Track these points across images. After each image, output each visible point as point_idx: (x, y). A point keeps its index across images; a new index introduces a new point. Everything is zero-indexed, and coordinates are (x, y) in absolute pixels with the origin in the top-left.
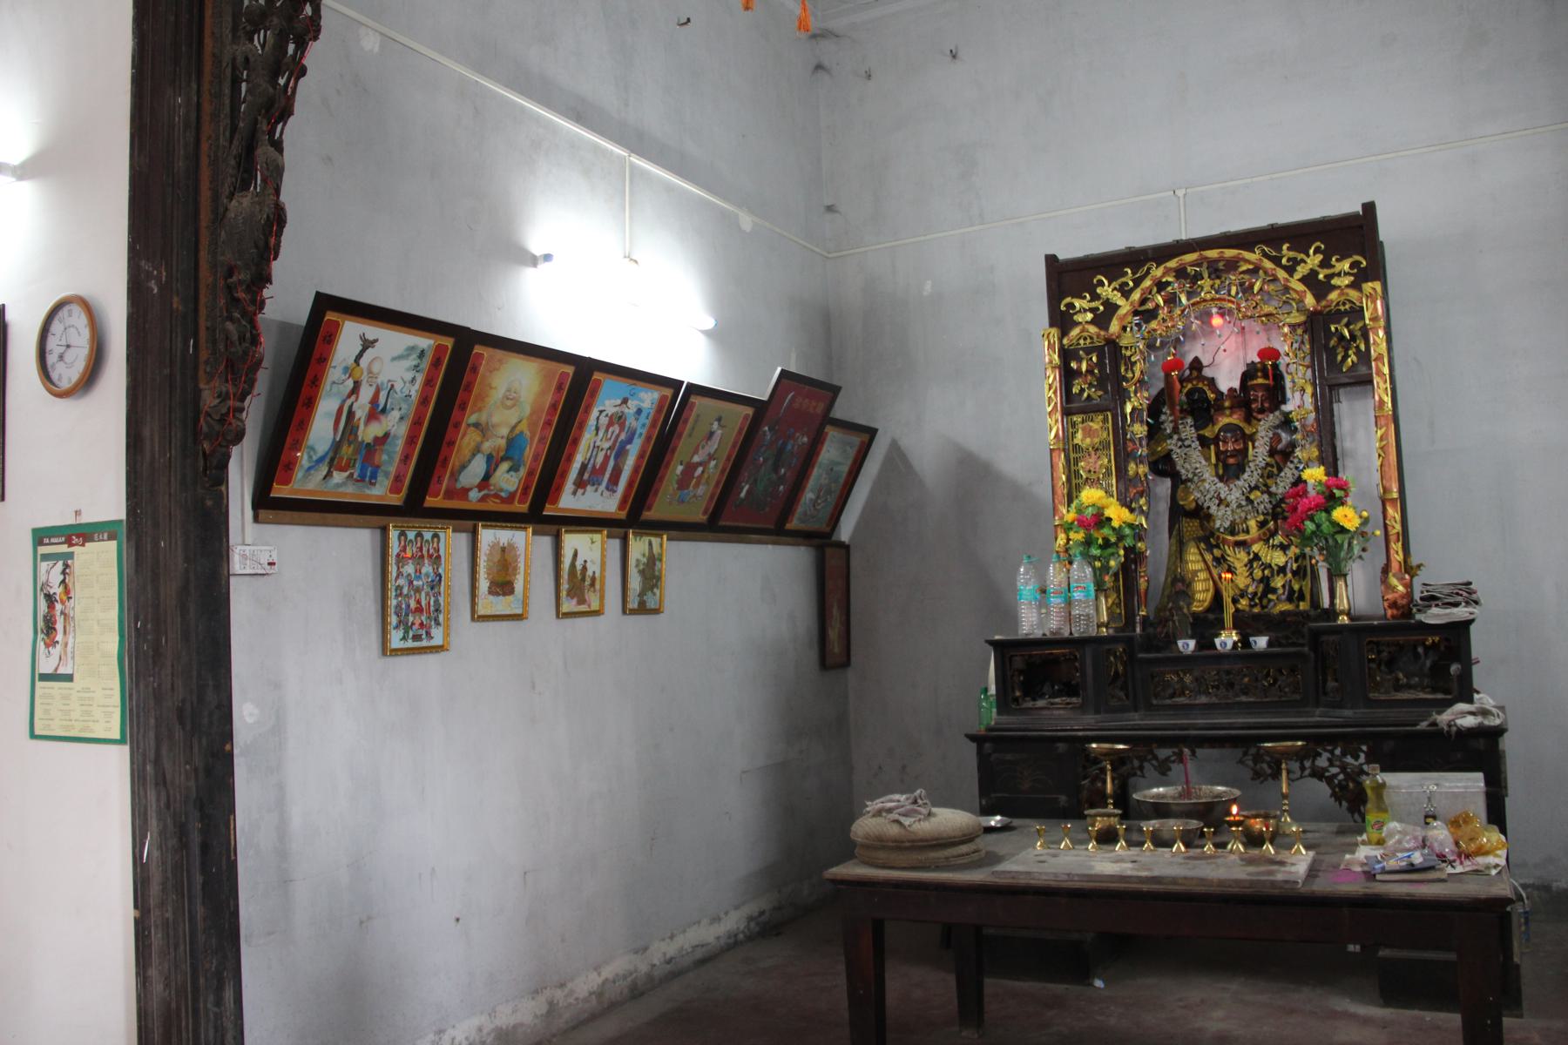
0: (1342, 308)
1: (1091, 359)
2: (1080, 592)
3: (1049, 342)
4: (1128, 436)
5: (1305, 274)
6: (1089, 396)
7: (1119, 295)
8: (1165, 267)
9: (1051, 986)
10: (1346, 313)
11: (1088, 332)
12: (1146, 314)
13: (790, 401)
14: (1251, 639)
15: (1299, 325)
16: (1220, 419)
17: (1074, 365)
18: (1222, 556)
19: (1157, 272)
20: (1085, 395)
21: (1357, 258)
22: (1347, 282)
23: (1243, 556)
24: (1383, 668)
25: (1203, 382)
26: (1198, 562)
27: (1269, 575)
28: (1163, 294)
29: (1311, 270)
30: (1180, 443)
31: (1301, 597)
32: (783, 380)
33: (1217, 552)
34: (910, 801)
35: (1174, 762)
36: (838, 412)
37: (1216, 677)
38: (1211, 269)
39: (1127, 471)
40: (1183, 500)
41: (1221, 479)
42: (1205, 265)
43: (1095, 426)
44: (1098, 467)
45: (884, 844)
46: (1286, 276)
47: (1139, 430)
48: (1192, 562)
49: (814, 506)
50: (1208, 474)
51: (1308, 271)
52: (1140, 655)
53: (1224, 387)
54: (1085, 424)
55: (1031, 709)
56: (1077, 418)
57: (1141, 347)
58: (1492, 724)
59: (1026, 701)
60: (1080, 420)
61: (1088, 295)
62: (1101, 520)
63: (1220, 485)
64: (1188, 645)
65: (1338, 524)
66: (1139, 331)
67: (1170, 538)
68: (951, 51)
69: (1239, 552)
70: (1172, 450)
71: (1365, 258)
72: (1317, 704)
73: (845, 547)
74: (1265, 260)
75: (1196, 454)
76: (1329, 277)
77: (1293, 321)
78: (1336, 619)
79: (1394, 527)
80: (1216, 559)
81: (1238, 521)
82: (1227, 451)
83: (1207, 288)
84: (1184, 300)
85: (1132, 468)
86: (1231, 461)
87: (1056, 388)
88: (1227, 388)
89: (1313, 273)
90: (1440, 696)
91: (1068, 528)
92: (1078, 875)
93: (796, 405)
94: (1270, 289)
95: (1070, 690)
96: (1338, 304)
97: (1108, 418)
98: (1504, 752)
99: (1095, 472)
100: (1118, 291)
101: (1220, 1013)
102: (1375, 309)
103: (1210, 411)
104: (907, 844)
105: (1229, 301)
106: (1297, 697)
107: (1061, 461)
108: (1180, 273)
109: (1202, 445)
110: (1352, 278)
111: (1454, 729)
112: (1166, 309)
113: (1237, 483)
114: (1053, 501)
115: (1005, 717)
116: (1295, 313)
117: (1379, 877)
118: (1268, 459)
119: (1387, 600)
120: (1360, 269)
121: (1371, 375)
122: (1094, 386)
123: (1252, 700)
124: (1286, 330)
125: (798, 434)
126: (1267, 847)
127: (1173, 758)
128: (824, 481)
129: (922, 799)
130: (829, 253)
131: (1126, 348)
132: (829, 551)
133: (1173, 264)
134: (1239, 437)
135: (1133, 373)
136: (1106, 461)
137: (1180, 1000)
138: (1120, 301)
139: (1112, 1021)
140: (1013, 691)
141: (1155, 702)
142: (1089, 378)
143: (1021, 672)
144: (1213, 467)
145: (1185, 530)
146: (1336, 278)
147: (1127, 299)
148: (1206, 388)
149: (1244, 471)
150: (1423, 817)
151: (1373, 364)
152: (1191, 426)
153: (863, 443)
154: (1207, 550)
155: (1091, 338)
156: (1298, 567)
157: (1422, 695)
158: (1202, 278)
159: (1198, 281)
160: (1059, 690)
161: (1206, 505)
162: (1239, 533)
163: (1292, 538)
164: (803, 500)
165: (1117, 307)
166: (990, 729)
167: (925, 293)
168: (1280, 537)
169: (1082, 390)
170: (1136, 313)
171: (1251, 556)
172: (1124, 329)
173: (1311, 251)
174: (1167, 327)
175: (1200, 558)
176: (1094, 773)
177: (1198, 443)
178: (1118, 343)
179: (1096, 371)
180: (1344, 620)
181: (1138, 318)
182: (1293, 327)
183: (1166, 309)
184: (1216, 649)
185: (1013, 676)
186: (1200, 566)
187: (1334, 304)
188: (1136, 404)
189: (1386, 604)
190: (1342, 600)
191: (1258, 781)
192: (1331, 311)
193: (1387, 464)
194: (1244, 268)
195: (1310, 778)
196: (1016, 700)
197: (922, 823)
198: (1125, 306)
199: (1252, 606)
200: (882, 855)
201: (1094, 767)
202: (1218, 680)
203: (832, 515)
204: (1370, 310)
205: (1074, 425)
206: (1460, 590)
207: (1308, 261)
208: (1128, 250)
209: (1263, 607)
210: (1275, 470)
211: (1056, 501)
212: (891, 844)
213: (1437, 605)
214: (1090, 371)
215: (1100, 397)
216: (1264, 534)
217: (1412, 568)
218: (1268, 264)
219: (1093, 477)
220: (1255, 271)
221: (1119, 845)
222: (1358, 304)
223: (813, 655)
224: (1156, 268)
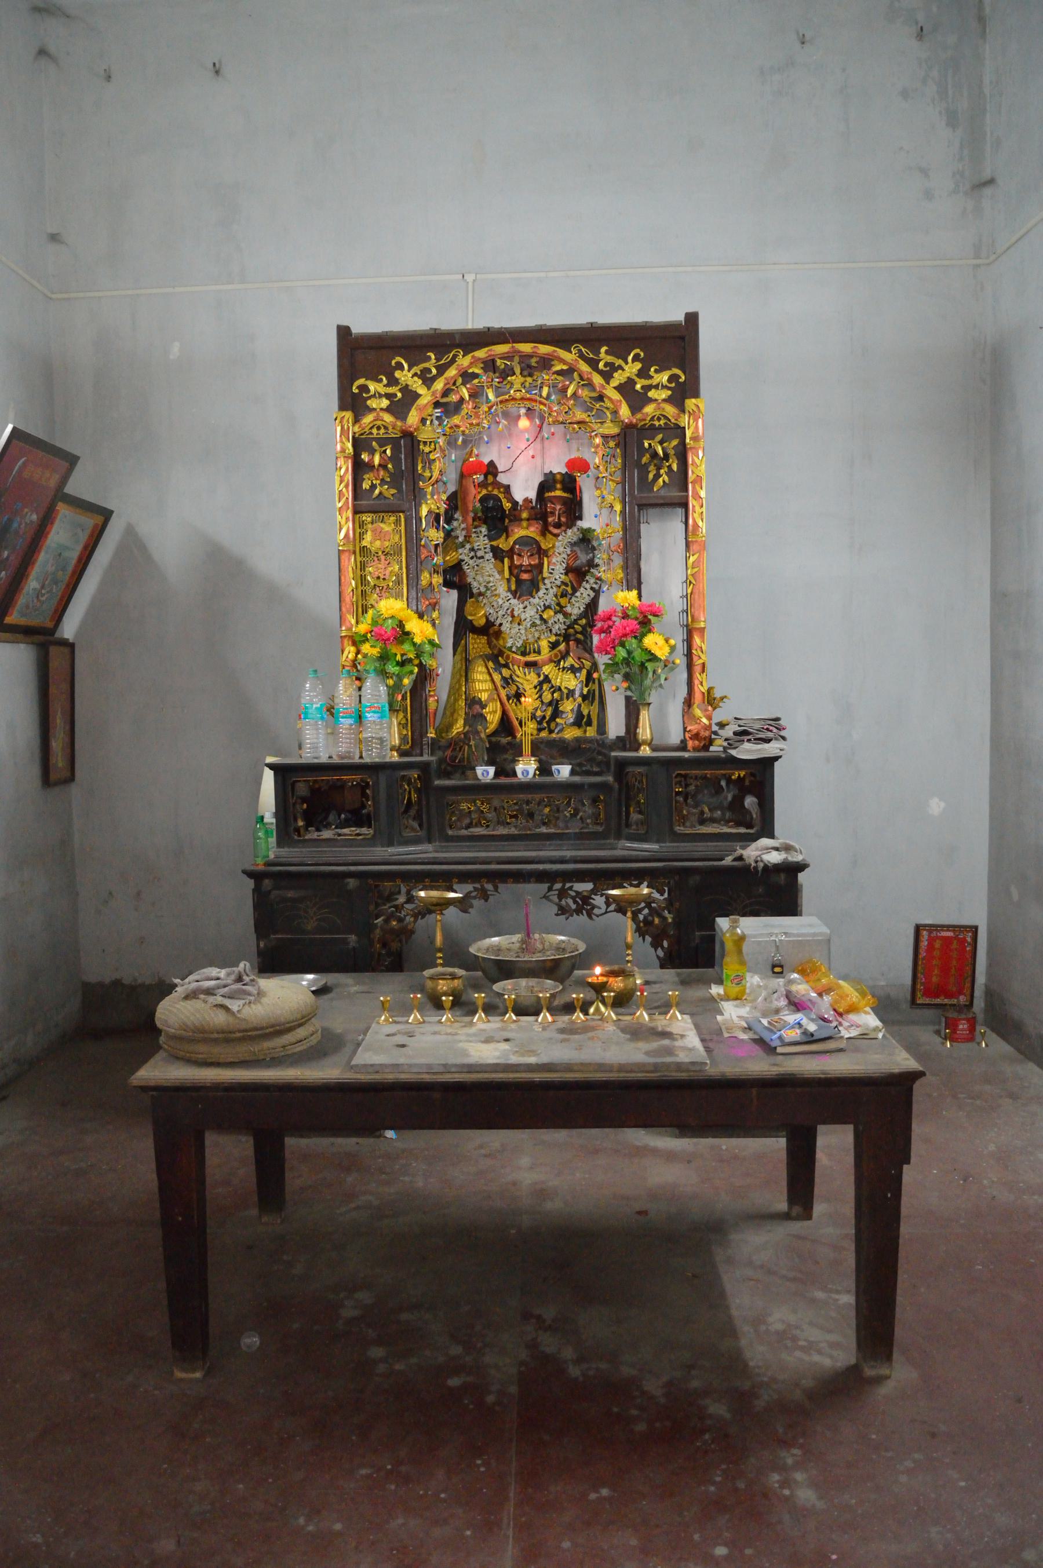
0: (657, 423)
1: (385, 451)
2: (374, 712)
3: (342, 428)
4: (423, 542)
5: (622, 382)
6: (381, 493)
7: (420, 382)
8: (473, 357)
9: (340, 1140)
10: (660, 428)
11: (383, 420)
12: (446, 407)
13: (20, 467)
14: (554, 767)
15: (613, 437)
16: (516, 530)
17: (365, 457)
18: (511, 676)
19: (464, 361)
20: (377, 492)
21: (676, 371)
22: (664, 396)
23: (533, 678)
24: (689, 801)
25: (498, 489)
26: (486, 681)
27: (559, 699)
28: (468, 386)
29: (628, 378)
30: (472, 554)
31: (589, 723)
32: (15, 441)
33: (506, 672)
34: (233, 977)
35: (475, 898)
36: (70, 489)
37: (517, 807)
38: (523, 365)
39: (418, 578)
40: (471, 615)
41: (514, 594)
42: (517, 359)
43: (387, 527)
44: (387, 573)
45: (206, 1035)
46: (602, 381)
47: (435, 536)
48: (479, 681)
49: (38, 597)
50: (502, 589)
51: (626, 380)
52: (437, 782)
53: (519, 496)
54: (375, 525)
55: (316, 840)
56: (367, 518)
57: (441, 444)
58: (795, 860)
59: (310, 832)
60: (369, 519)
61: (384, 379)
62: (403, 635)
63: (514, 601)
64: (486, 773)
65: (650, 651)
66: (439, 425)
67: (454, 654)
68: (214, 64)
69: (529, 673)
70: (464, 560)
71: (685, 374)
72: (619, 836)
73: (70, 646)
74: (581, 362)
75: (489, 565)
76: (647, 388)
77: (607, 432)
78: (637, 749)
79: (700, 658)
80: (504, 679)
81: (531, 640)
82: (521, 565)
83: (517, 386)
84: (491, 396)
85: (425, 578)
86: (525, 576)
87: (348, 480)
88: (523, 498)
89: (630, 382)
90: (742, 830)
91: (357, 641)
92: (456, 1065)
93: (26, 474)
94: (584, 395)
95: (358, 819)
96: (652, 419)
97: (400, 521)
98: (802, 886)
99: (384, 579)
100: (419, 377)
101: (525, 1161)
102: (697, 427)
103: (504, 521)
104: (238, 1035)
105: (541, 403)
106: (600, 829)
107: (350, 563)
108: (490, 365)
109: (495, 557)
110: (670, 393)
111: (761, 865)
112: (471, 403)
113: (532, 600)
114: (340, 610)
115: (286, 849)
116: (609, 424)
117: (779, 1050)
118: (563, 577)
119: (689, 731)
120: (678, 383)
121: (687, 497)
122: (387, 483)
123: (552, 831)
124: (597, 441)
125: (26, 510)
126: (642, 1014)
127: (474, 894)
128: (51, 569)
129: (247, 975)
130: (53, 293)
131: (425, 443)
132: (53, 650)
133: (481, 353)
134: (535, 552)
135: (431, 472)
136: (397, 567)
137: (481, 1147)
138: (422, 390)
139: (420, 1183)
140: (296, 820)
141: (450, 832)
142: (382, 473)
143: (304, 800)
144: (505, 581)
145: (471, 647)
146: (653, 391)
147: (429, 388)
148: (501, 496)
149: (538, 590)
150: (784, 972)
151: (690, 486)
152: (485, 536)
153: (96, 526)
154: (495, 670)
155: (386, 428)
156: (589, 691)
157: (726, 830)
158: (514, 374)
159: (508, 377)
160: (346, 820)
161: (498, 622)
162: (529, 653)
163: (584, 661)
164: (25, 591)
165: (417, 396)
166: (268, 864)
167: (171, 357)
168: (571, 659)
169: (373, 487)
170: (437, 404)
171: (542, 678)
172: (423, 421)
173: (630, 358)
174: (471, 424)
175: (488, 678)
176: (389, 911)
177: (491, 554)
178: (416, 437)
179: (390, 466)
180: (645, 751)
181: (439, 410)
182: (605, 437)
183: (471, 403)
184: (516, 776)
185: (294, 804)
186: (488, 685)
187: (649, 419)
188: (432, 506)
189: (687, 735)
190: (644, 729)
191: (563, 917)
192: (645, 424)
193: (697, 591)
194: (558, 367)
195: (615, 913)
196: (297, 830)
197: (252, 1005)
198: (426, 397)
199: (540, 730)
200: (203, 1050)
201: (388, 905)
202: (516, 810)
203: (56, 611)
204: (692, 428)
205: (362, 525)
206: (771, 726)
207: (626, 368)
208: (433, 332)
209: (551, 732)
210: (569, 589)
211: (344, 609)
212: (216, 1035)
213: (749, 740)
214: (383, 466)
215: (392, 495)
216: (556, 655)
217: (714, 699)
218: (584, 367)
219: (383, 584)
220: (568, 373)
221: (477, 1016)
222: (673, 420)
223: (35, 771)
224: (463, 356)
